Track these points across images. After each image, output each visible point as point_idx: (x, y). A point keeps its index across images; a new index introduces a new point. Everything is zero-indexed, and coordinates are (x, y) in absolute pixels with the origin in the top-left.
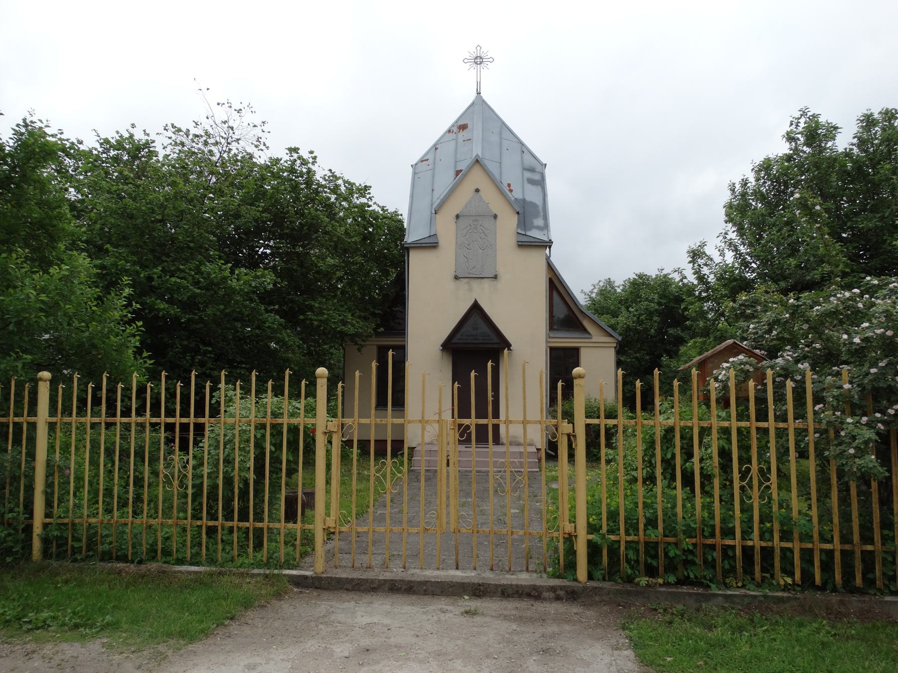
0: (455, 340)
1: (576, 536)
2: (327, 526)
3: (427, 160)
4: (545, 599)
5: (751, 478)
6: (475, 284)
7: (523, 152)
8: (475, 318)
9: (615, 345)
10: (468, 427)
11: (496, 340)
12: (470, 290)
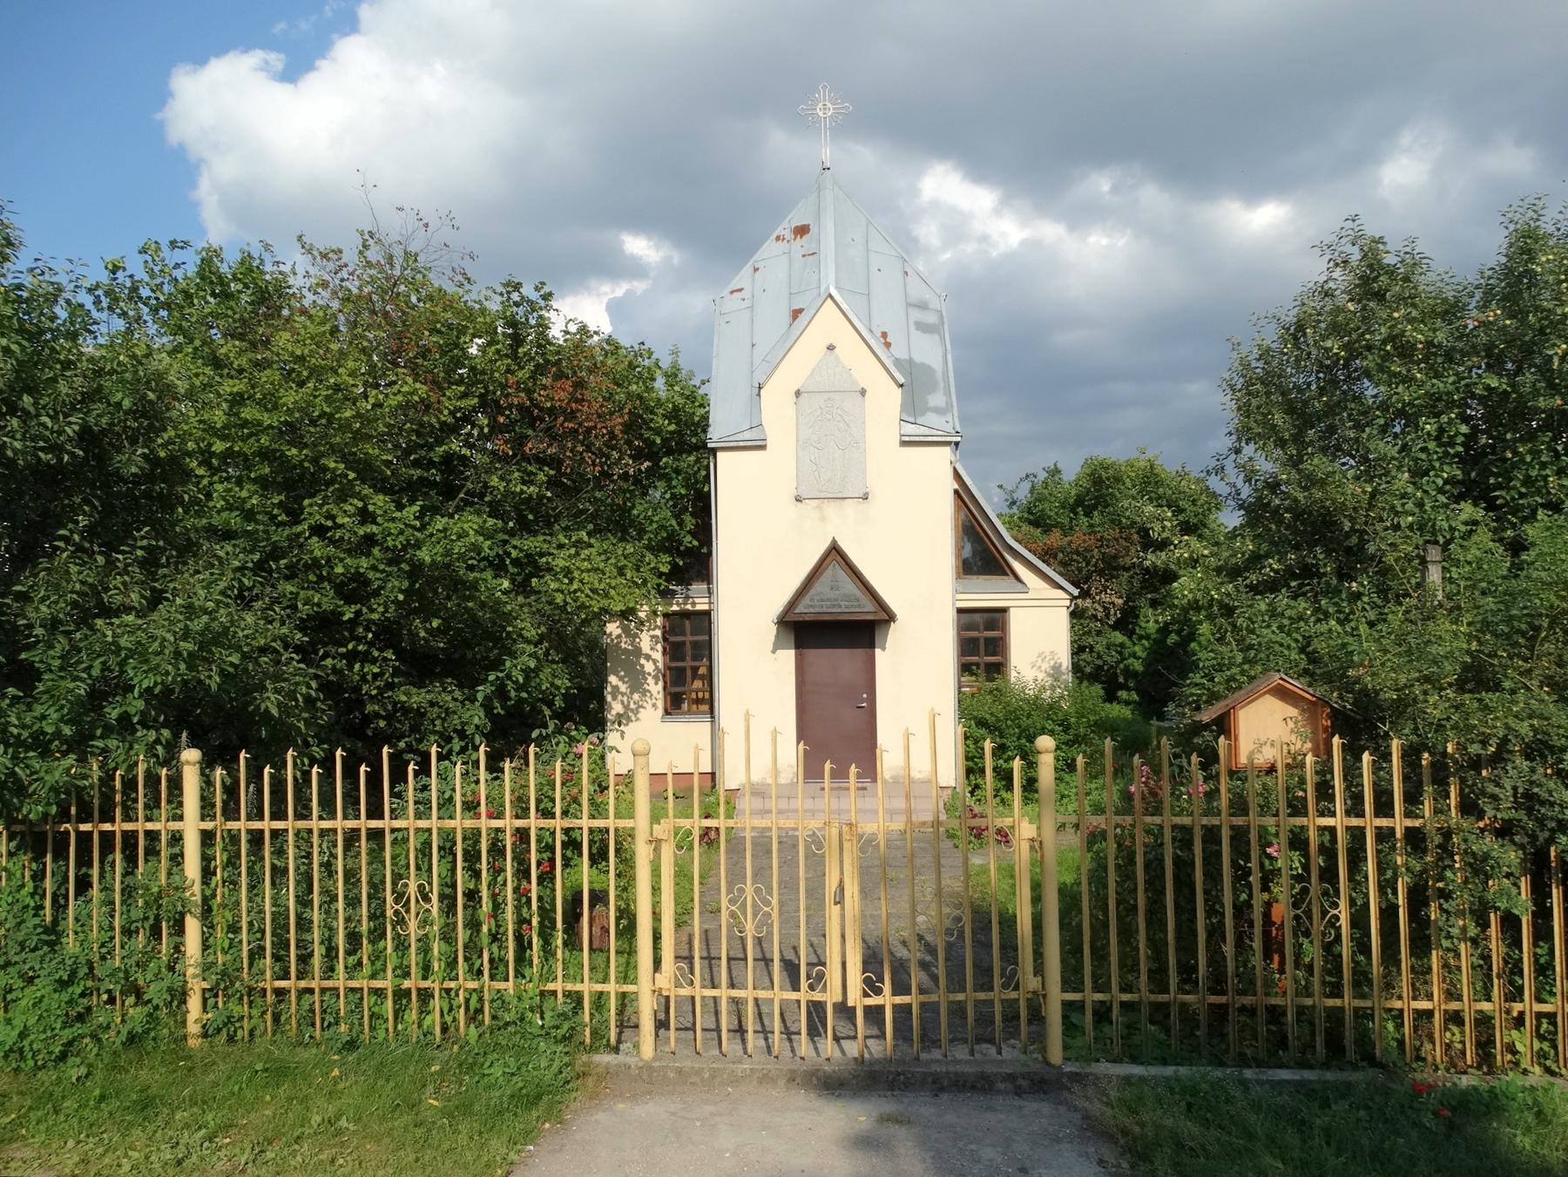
0: (800, 609)
1: (1045, 996)
2: (657, 986)
3: (740, 290)
4: (999, 1092)
5: (1310, 903)
6: (831, 509)
7: (906, 273)
8: (835, 571)
9: (1067, 603)
10: (1005, 986)
11: (869, 606)
12: (823, 519)
